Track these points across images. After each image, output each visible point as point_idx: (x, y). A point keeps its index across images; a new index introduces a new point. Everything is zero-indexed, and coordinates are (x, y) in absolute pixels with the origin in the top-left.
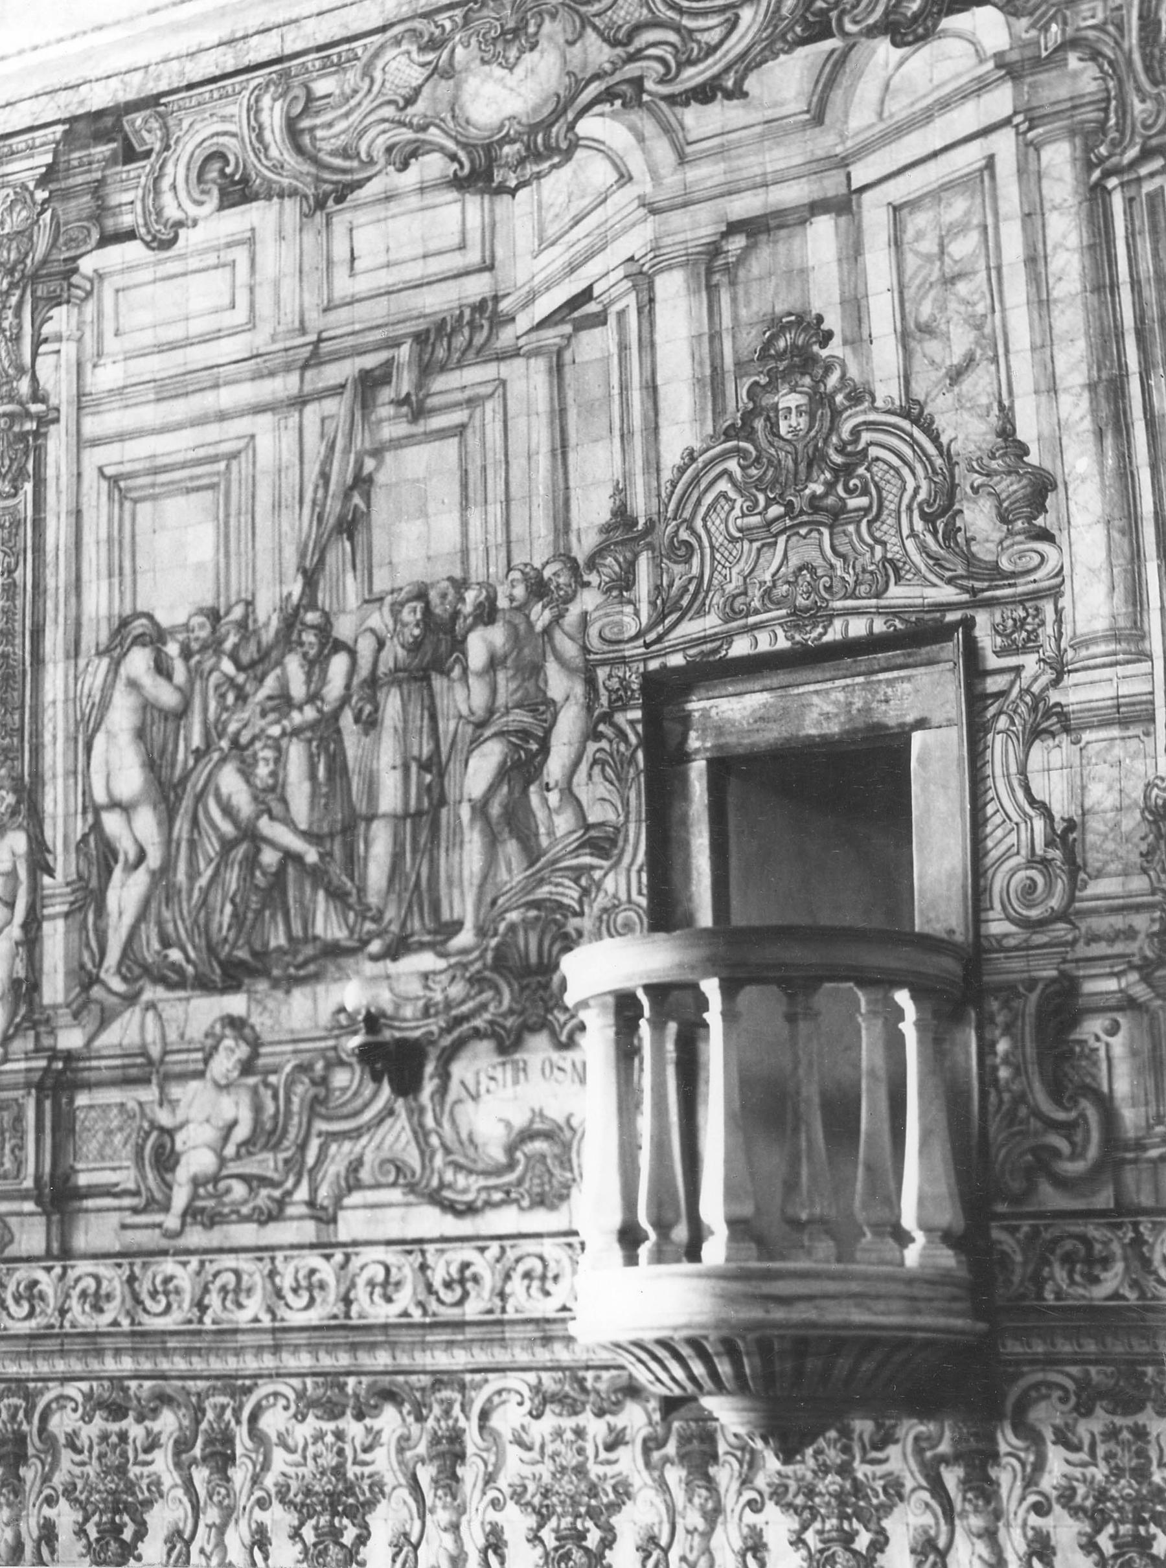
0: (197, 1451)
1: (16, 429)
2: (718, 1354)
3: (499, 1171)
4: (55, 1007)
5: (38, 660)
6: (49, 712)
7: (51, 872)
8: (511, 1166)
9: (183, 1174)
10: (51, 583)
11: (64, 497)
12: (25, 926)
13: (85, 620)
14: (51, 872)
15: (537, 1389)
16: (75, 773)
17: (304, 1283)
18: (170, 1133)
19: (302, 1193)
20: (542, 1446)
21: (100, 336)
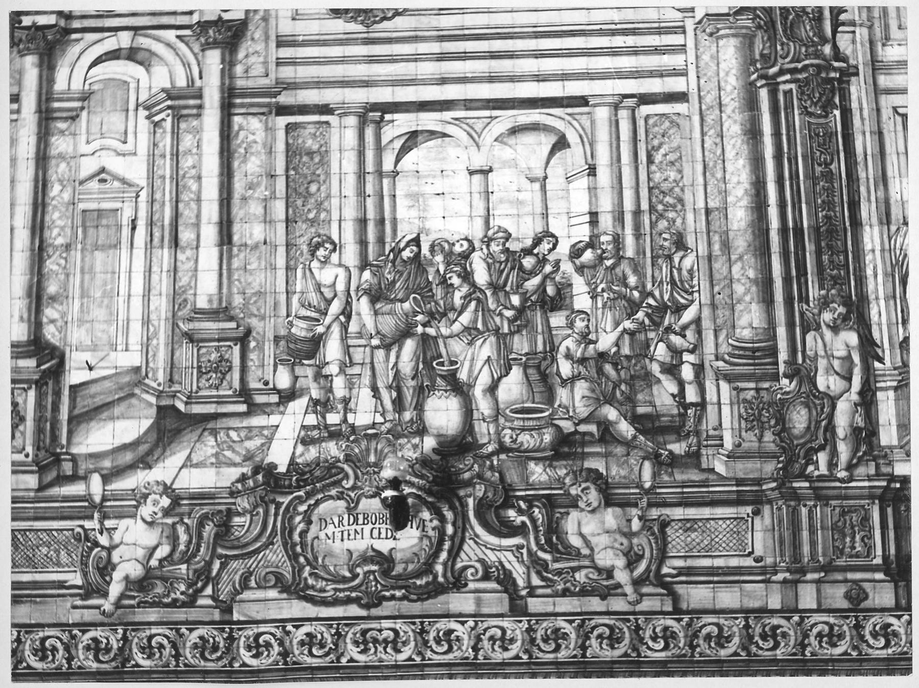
1: (823, 75)
4: (891, 448)
5: (856, 223)
6: (869, 258)
7: (881, 360)
8: (355, 576)
9: (117, 575)
10: (862, 175)
11: (867, 122)
12: (861, 393)
13: (892, 201)
14: (881, 360)
16: (894, 297)
18: (110, 550)
19: (209, 591)
21: (887, 27)
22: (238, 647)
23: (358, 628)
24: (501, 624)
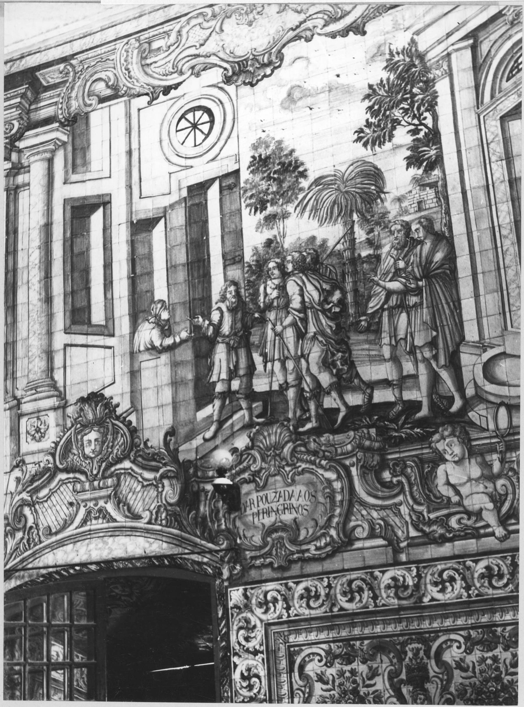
0: (403, 676)
2: (454, 622)
3: (261, 548)
8: (265, 544)
15: (467, 638)
17: (271, 605)
20: (334, 681)
22: (425, 584)
23: (344, 580)
24: (313, 612)
